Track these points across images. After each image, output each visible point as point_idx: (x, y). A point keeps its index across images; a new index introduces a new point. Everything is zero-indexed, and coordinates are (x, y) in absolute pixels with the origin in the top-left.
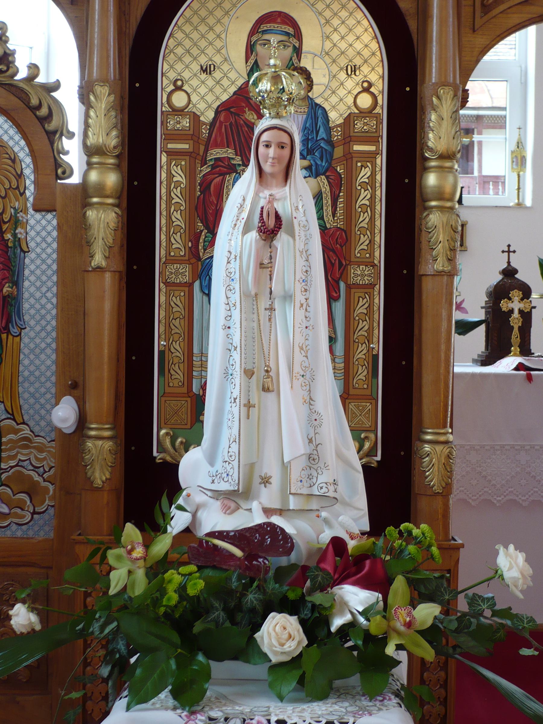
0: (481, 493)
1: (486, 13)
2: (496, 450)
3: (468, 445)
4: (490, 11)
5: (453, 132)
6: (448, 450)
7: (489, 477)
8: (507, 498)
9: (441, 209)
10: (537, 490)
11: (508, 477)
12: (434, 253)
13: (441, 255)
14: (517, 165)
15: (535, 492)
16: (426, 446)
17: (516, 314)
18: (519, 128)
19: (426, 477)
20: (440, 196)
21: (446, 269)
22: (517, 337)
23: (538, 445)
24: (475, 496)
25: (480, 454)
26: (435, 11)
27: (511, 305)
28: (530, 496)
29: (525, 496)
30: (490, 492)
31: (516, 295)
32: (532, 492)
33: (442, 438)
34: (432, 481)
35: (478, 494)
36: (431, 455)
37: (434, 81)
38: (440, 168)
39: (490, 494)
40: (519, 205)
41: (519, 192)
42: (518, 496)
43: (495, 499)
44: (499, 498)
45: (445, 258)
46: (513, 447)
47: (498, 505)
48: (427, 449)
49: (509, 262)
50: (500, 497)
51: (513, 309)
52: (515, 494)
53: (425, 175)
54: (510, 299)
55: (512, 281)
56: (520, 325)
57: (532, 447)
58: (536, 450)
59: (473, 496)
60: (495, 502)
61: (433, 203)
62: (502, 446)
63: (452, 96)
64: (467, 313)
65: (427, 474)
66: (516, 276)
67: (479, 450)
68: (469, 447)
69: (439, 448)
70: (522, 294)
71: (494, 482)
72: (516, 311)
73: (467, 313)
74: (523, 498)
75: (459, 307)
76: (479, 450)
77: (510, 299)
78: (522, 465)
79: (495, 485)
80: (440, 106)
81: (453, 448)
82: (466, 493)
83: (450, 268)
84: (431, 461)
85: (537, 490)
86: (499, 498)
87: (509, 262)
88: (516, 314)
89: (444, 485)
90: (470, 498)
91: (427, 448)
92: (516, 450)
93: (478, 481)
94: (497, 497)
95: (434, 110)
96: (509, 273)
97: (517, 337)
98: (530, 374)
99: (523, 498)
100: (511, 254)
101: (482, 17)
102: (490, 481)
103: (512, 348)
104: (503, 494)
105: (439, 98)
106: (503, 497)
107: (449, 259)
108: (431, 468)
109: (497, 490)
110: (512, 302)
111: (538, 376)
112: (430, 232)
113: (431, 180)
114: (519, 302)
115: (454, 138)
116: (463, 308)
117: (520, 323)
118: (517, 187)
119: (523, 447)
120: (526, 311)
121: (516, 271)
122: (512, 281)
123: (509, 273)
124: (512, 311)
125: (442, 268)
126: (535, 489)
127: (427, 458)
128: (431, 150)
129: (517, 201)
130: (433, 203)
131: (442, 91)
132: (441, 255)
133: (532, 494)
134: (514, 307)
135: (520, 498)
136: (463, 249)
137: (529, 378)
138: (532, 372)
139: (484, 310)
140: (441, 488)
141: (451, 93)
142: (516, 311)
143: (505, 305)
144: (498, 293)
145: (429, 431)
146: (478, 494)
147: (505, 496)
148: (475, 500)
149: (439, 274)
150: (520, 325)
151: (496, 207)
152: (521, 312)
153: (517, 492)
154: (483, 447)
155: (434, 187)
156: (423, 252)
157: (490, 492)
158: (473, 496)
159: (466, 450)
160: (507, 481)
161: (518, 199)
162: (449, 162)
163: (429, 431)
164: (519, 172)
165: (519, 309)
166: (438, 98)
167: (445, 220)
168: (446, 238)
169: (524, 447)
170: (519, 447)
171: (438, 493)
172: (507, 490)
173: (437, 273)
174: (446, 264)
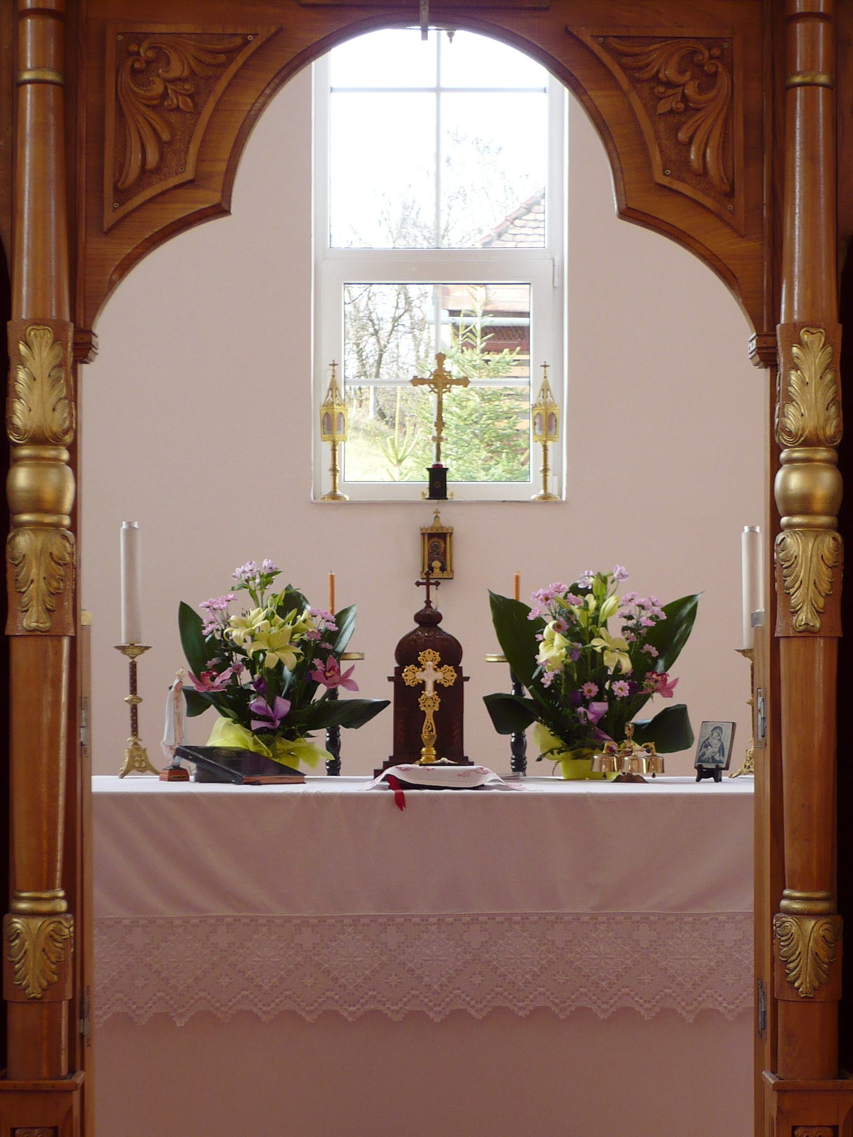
0: (405, 1000)
1: (122, 203)
2: (515, 923)
3: (298, 917)
4: (129, 199)
5: (53, 398)
6: (51, 927)
7: (165, 974)
8: (368, 1007)
9: (38, 526)
10: (417, 992)
11: (367, 972)
12: (25, 599)
13: (34, 602)
14: (541, 429)
15: (413, 996)
16: (15, 920)
17: (429, 691)
18: (545, 366)
19: (16, 973)
20: (37, 505)
21: (41, 625)
22: (432, 731)
23: (416, 916)
24: (311, 1005)
25: (740, 929)
26: (26, 203)
27: (420, 676)
28: (277, 1005)
29: (397, 1004)
30: (337, 997)
31: (429, 658)
32: (409, 996)
33: (45, 907)
34: (24, 979)
35: (316, 1001)
36: (21, 936)
37: (24, 317)
38: (37, 459)
39: (337, 1002)
40: (546, 497)
41: (545, 476)
42: (384, 1005)
43: (346, 1009)
44: (352, 1009)
45: (40, 608)
46: (374, 919)
47: (350, 1019)
48: (18, 926)
49: (428, 602)
50: (354, 1006)
51: (424, 682)
52: (380, 1001)
53: (11, 471)
54: (419, 665)
55: (431, 634)
56: (437, 709)
57: (408, 919)
58: (414, 924)
59: (307, 1005)
60: (345, 1014)
61: (26, 517)
62: (356, 920)
63: (50, 341)
64: (357, 689)
65: (17, 966)
66: (439, 625)
67: (486, 923)
68: (299, 921)
69: (38, 922)
70: (440, 656)
71: (342, 981)
72: (430, 686)
73: (357, 689)
74: (395, 1008)
75: (345, 680)
76: (486, 923)
77: (419, 665)
78: (390, 950)
79: (345, 986)
80: (31, 358)
81: (60, 923)
82: (295, 1001)
83: (48, 625)
84: (22, 944)
85: (417, 992)
86: (352, 1009)
87: (428, 602)
88: (429, 691)
89: (45, 984)
90: (641, 1006)
91: (18, 924)
92: (380, 924)
93: (315, 979)
94: (350, 1006)
95: (22, 365)
96: (428, 619)
97: (432, 731)
98: (402, 794)
99: (395, 1008)
100: (432, 588)
101: (114, 210)
102: (337, 979)
103: (423, 750)
104: (358, 1002)
105: (28, 345)
106: (358, 1006)
107: (48, 610)
108: (23, 956)
109: (349, 994)
110: (424, 670)
111: (416, 797)
112: (17, 565)
113: (22, 478)
114: (435, 670)
115: (54, 410)
116: (351, 681)
117: (437, 705)
118: (542, 468)
119: (391, 919)
120: (446, 685)
121: (438, 617)
122: (431, 634)
123: (428, 619)
124: (422, 686)
125: (35, 624)
126: (582, 990)
127: (17, 941)
128: (17, 430)
129: (542, 492)
130: (26, 517)
131: (32, 333)
132: (34, 602)
133: (409, 1000)
134: (426, 679)
135: (389, 1008)
136: (445, 575)
137: (400, 801)
138: (405, 792)
139: (392, 683)
140: (39, 990)
141: (49, 336)
142: (430, 686)
143: (411, 676)
144: (407, 653)
145: (24, 895)
146: (316, 1001)
147: (363, 1005)
148: (312, 1012)
149: (32, 633)
150: (437, 709)
151: (504, 501)
152: (437, 686)
153: (383, 997)
154: (323, 920)
155: (24, 491)
156: (10, 597)
157: (337, 997)
158: (307, 1005)
159: (295, 925)
160: (365, 979)
161: (545, 488)
162: (53, 449)
163: (24, 895)
164: (545, 442)
165: (435, 682)
166: (28, 345)
167: (39, 544)
168: (42, 575)
169: (561, 918)
170: (469, 919)
171: (34, 998)
172: (366, 994)
173: (28, 633)
174: (44, 617)
